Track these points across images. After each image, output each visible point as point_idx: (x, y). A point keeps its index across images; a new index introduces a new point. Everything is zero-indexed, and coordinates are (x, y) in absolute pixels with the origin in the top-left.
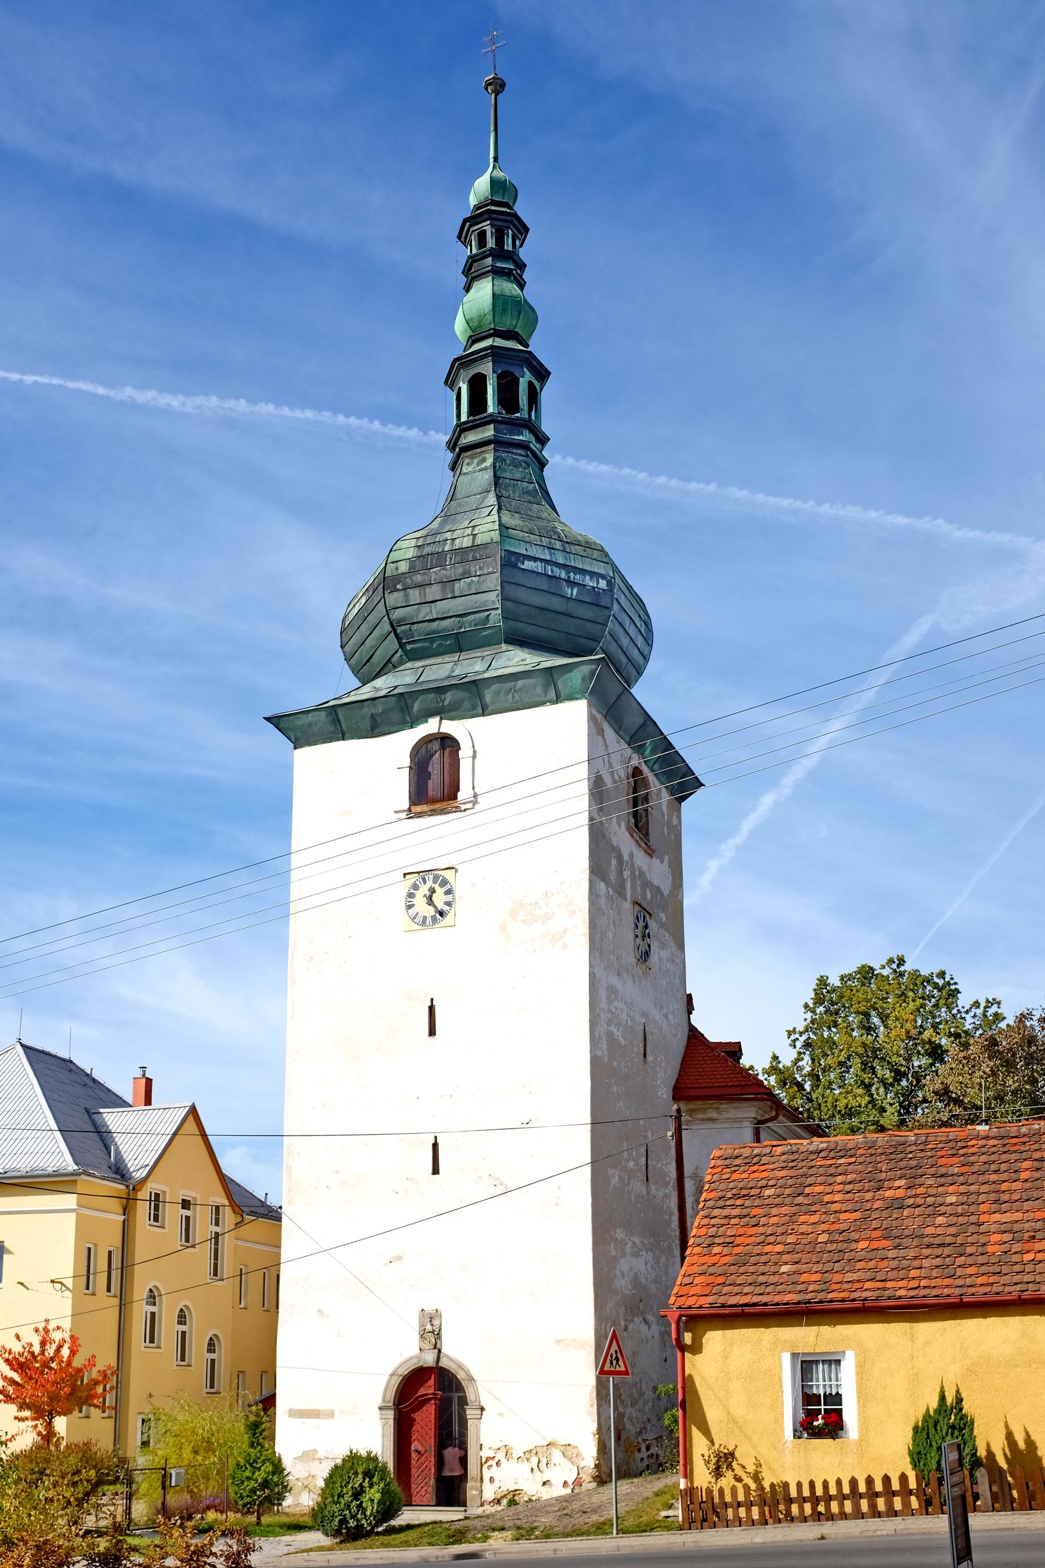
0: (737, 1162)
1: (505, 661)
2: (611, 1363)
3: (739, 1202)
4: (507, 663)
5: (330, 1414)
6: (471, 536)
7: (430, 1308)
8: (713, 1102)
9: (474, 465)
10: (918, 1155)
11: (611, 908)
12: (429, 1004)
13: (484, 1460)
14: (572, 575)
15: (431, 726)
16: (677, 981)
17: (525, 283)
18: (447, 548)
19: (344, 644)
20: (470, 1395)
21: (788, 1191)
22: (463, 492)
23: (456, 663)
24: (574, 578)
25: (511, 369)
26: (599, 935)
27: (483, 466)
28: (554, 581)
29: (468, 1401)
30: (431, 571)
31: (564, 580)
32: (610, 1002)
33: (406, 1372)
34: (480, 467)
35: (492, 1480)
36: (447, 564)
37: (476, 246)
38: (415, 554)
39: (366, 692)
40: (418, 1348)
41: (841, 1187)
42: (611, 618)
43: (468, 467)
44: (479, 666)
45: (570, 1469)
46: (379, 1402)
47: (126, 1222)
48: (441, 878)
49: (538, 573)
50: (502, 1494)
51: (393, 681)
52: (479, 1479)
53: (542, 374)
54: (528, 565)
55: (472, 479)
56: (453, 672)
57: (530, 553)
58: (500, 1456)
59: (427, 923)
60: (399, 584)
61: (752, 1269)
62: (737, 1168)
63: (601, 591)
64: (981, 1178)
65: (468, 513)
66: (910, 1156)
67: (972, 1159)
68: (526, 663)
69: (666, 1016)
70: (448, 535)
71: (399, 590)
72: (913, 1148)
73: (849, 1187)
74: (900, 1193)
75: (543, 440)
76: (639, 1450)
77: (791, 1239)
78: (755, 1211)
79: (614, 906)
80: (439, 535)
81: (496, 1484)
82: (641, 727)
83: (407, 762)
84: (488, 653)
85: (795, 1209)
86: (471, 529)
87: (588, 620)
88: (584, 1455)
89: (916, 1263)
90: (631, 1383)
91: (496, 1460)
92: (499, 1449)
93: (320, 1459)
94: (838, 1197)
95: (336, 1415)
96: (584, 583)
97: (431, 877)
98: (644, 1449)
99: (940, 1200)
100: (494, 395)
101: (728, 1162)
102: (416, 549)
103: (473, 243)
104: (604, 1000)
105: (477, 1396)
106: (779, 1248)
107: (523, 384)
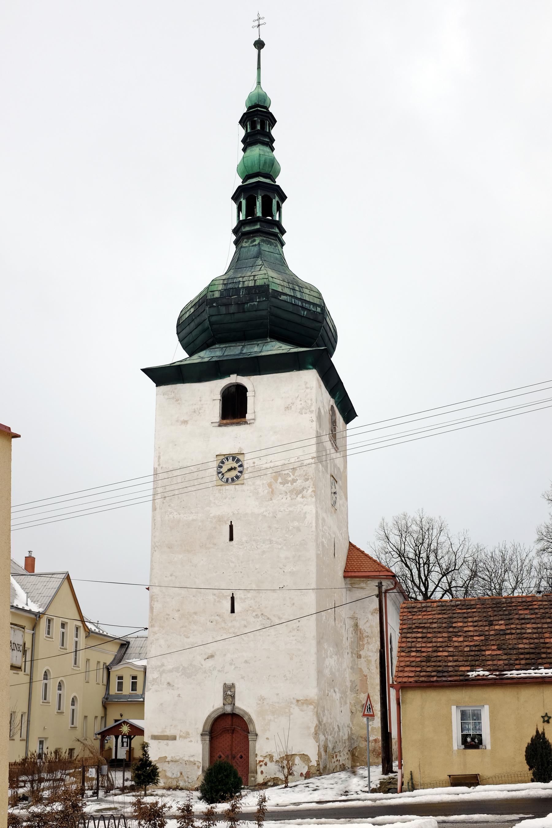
0: (415, 610)
1: (271, 347)
2: (368, 710)
3: (420, 630)
4: (272, 348)
5: (174, 738)
6: (253, 281)
7: (229, 682)
8: (364, 579)
9: (249, 243)
10: (508, 608)
11: (323, 478)
12: (230, 524)
13: (258, 762)
14: (304, 304)
15: (234, 379)
16: (345, 516)
17: (274, 149)
18: (240, 286)
19: (179, 331)
20: (250, 728)
21: (444, 625)
22: (244, 256)
23: (244, 346)
24: (305, 306)
25: (268, 194)
26: (319, 492)
27: (254, 244)
28: (296, 307)
29: (250, 731)
30: (232, 297)
31: (300, 306)
32: (323, 526)
33: (216, 716)
34: (252, 244)
35: (262, 772)
36: (241, 294)
37: (249, 128)
38: (223, 288)
39: (196, 359)
40: (223, 703)
41: (471, 624)
42: (322, 328)
43: (245, 244)
44: (256, 349)
45: (304, 767)
46: (200, 730)
47: (34, 635)
48: (236, 458)
49: (288, 302)
50: (268, 780)
51: (210, 353)
52: (255, 772)
53: (283, 198)
54: (283, 297)
55: (248, 250)
56: (243, 351)
57: (284, 292)
58: (267, 760)
59: (229, 482)
60: (214, 303)
61: (433, 664)
62: (415, 613)
63: (318, 313)
64: (543, 621)
65: (248, 268)
66: (504, 609)
67: (536, 611)
68: (281, 348)
69: (341, 534)
70: (241, 279)
71: (214, 306)
72: (505, 605)
73: (475, 624)
74: (503, 627)
75: (283, 232)
76: (333, 757)
77: (451, 649)
78: (429, 635)
79: (324, 477)
80: (235, 279)
81: (264, 775)
82: (335, 385)
83: (219, 397)
84: (260, 342)
85: (450, 634)
86: (252, 277)
87: (312, 329)
88: (311, 759)
89: (517, 662)
90: (330, 723)
91: (264, 762)
92: (266, 756)
93: (168, 762)
94: (471, 629)
95: (178, 738)
96: (310, 309)
97: (231, 458)
98: (335, 757)
99: (523, 631)
100: (260, 207)
101: (410, 610)
102: (223, 286)
103: (248, 127)
104: (321, 525)
105: (254, 728)
106: (446, 654)
107: (274, 202)
